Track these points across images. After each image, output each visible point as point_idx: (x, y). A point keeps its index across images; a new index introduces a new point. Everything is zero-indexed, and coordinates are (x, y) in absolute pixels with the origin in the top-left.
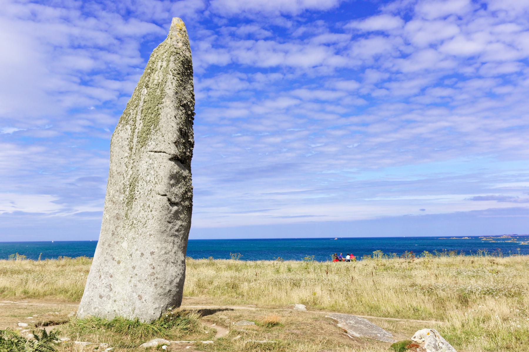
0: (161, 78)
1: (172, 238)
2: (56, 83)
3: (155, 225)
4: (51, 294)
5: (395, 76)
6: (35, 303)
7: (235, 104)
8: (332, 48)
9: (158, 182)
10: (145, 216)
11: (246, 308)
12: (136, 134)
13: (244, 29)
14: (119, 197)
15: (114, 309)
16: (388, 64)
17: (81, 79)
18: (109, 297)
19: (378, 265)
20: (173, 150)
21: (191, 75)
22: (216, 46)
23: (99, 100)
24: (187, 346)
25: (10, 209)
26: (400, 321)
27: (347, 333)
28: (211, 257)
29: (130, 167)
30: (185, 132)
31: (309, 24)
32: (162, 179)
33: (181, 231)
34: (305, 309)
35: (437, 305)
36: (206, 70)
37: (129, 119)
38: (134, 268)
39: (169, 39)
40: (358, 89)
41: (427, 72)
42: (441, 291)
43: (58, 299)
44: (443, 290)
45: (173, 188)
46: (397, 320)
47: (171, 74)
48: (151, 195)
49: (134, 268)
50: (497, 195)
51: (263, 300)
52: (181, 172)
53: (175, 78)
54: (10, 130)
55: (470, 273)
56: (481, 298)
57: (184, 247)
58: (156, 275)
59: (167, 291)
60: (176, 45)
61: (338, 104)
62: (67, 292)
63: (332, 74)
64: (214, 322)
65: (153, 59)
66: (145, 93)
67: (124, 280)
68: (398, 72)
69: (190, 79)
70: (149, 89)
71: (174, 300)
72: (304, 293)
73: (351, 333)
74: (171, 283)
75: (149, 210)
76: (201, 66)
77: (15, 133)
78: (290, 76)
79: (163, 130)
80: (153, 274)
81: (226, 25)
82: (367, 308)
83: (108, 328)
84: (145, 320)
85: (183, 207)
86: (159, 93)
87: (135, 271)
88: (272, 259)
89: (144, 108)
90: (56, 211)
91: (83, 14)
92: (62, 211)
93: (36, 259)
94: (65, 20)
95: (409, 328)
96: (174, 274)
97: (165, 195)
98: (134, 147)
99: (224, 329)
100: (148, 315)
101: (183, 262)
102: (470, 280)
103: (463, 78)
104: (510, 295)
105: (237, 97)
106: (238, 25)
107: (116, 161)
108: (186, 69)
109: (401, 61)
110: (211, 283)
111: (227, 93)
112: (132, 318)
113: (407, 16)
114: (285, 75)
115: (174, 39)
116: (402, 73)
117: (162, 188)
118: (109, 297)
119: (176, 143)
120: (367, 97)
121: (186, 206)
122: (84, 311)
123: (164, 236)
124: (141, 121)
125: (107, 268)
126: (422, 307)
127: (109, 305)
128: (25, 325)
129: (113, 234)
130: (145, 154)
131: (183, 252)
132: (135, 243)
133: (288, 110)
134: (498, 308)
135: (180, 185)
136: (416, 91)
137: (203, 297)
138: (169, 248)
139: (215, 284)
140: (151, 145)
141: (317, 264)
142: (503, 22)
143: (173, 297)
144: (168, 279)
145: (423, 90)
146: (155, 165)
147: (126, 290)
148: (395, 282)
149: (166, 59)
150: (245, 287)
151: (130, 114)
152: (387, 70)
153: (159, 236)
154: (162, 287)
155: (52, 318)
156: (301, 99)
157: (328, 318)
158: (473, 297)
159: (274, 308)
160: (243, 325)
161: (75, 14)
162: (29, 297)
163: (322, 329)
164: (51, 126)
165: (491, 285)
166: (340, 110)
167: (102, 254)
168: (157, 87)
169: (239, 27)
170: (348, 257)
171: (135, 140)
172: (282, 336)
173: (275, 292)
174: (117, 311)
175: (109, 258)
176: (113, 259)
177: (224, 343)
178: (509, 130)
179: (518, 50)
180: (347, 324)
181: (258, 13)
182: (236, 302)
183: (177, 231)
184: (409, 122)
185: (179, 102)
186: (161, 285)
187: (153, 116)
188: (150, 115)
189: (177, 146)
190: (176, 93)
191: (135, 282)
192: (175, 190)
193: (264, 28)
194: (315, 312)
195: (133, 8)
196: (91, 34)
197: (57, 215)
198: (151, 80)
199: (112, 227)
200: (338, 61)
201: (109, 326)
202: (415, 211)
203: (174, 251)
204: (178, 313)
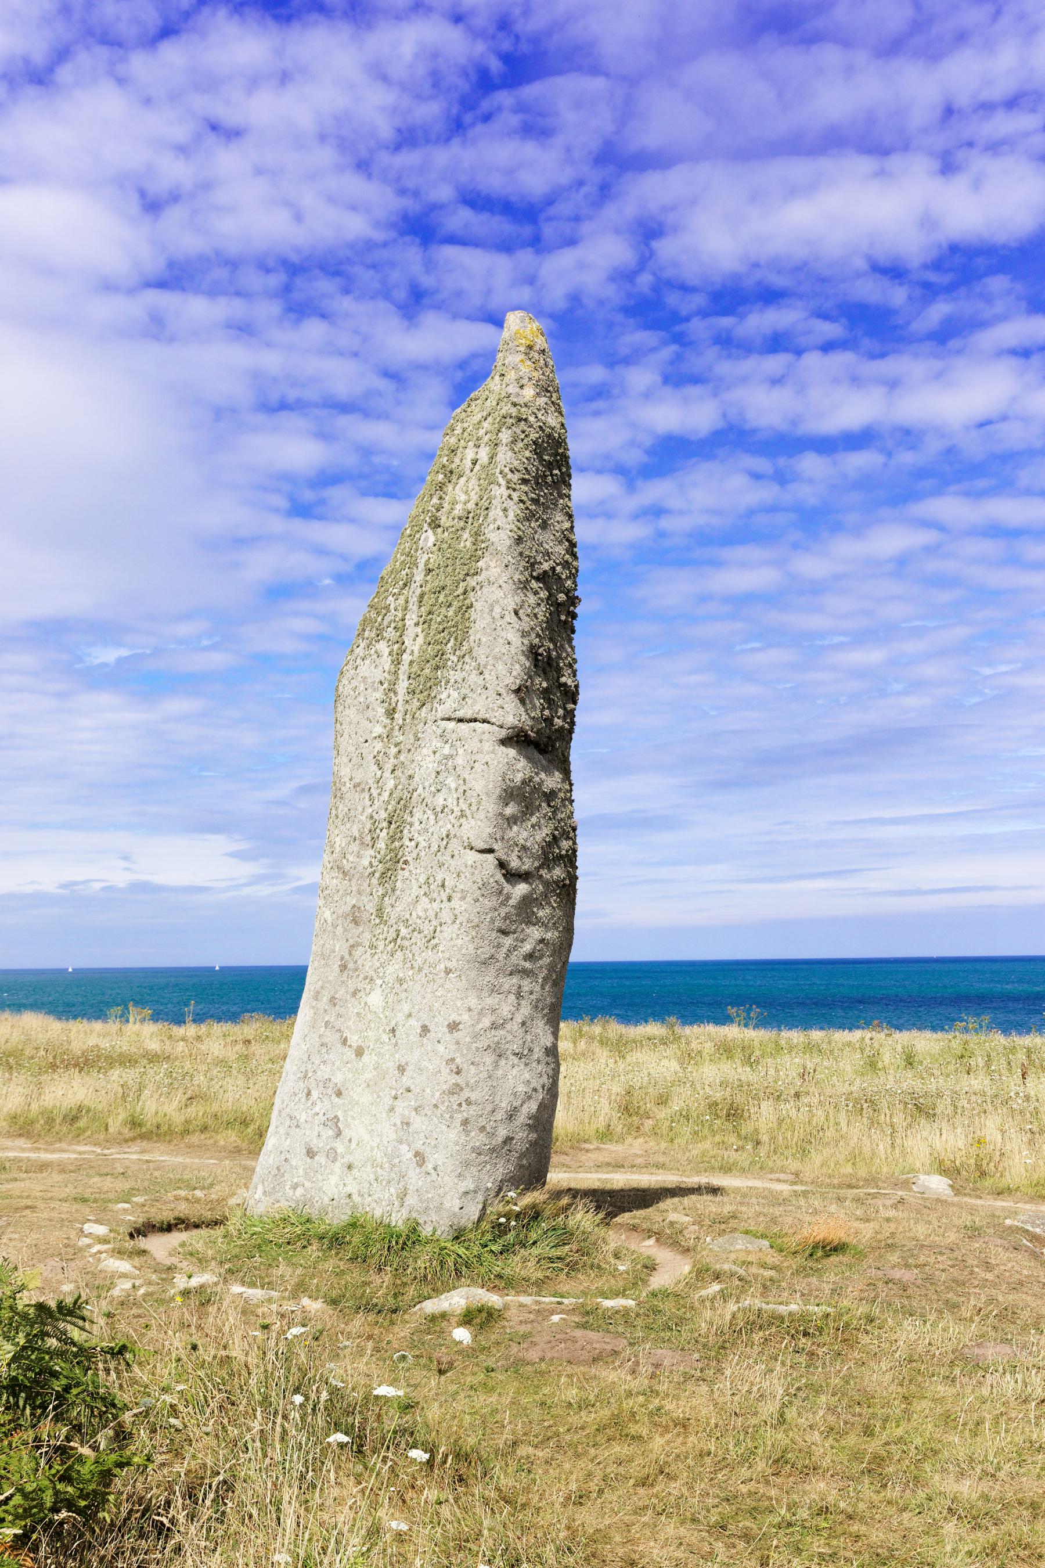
0: (475, 498)
1: (515, 980)
2: (226, 514)
3: (460, 942)
4: (205, 1129)
6: (161, 1155)
7: (739, 552)
9: (468, 813)
10: (431, 914)
11: (758, 1184)
12: (404, 668)
15: (349, 1189)
17: (292, 499)
18: (333, 1155)
20: (512, 714)
22: (678, 379)
23: (344, 558)
24: (552, 1312)
28: (673, 1019)
29: (388, 767)
30: (549, 657)
31: (962, 291)
32: (479, 803)
33: (541, 958)
34: (949, 1192)
36: (648, 452)
37: (385, 623)
38: (402, 1069)
39: (497, 377)
43: (222, 1143)
45: (515, 828)
48: (449, 850)
49: (402, 1069)
52: (537, 779)
54: (110, 655)
58: (466, 1094)
59: (500, 1140)
62: (245, 1123)
64: (649, 1233)
65: (453, 440)
67: (375, 1105)
69: (561, 496)
70: (440, 530)
71: (521, 1166)
72: (952, 1140)
74: (511, 1116)
75: (444, 896)
76: (633, 443)
77: (120, 661)
78: (907, 458)
79: (481, 653)
80: (456, 1089)
81: (703, 313)
83: (330, 1249)
84: (435, 1225)
85: (547, 884)
86: (468, 544)
87: (405, 1079)
88: (868, 1025)
89: (426, 589)
90: (243, 881)
91: (290, 309)
94: (240, 329)
96: (521, 1089)
97: (491, 851)
98: (400, 707)
99: (679, 1257)
100: (446, 1214)
101: (552, 1052)
105: (742, 532)
106: (741, 309)
107: (351, 749)
108: (550, 466)
110: (663, 1101)
112: (398, 1220)
114: (890, 455)
115: (511, 376)
117: (478, 828)
118: (333, 1155)
119: (521, 692)
121: (556, 882)
124: (419, 629)
125: (328, 1070)
127: (334, 1180)
128: (101, 1230)
129: (343, 968)
130: (430, 728)
131: (547, 1022)
132: (403, 995)
133: (902, 563)
135: (534, 820)
137: (636, 1146)
138: (505, 1010)
140: (448, 701)
141: (999, 1039)
143: (520, 1158)
144: (503, 1105)
146: (460, 761)
147: (381, 1136)
149: (486, 438)
150: (764, 1116)
151: (387, 608)
153: (473, 974)
154: (483, 1129)
155: (183, 1209)
159: (850, 1186)
160: (731, 1251)
161: (269, 310)
162: (142, 1137)
163: (988, 1266)
164: (217, 639)
168: (462, 523)
169: (742, 317)
171: (403, 686)
172: (853, 1291)
173: (856, 1131)
174: (355, 1197)
175: (332, 1037)
176: (345, 1042)
177: (668, 1307)
181: (799, 268)
182: (735, 1163)
183: (530, 957)
185: (526, 568)
186: (482, 1122)
187: (451, 613)
188: (443, 610)
189: (522, 701)
190: (519, 540)
191: (406, 1112)
192: (520, 833)
193: (824, 316)
194: (979, 1202)
195: (427, 281)
196: (313, 365)
197: (246, 891)
198: (446, 505)
199: (341, 947)
201: (335, 1241)
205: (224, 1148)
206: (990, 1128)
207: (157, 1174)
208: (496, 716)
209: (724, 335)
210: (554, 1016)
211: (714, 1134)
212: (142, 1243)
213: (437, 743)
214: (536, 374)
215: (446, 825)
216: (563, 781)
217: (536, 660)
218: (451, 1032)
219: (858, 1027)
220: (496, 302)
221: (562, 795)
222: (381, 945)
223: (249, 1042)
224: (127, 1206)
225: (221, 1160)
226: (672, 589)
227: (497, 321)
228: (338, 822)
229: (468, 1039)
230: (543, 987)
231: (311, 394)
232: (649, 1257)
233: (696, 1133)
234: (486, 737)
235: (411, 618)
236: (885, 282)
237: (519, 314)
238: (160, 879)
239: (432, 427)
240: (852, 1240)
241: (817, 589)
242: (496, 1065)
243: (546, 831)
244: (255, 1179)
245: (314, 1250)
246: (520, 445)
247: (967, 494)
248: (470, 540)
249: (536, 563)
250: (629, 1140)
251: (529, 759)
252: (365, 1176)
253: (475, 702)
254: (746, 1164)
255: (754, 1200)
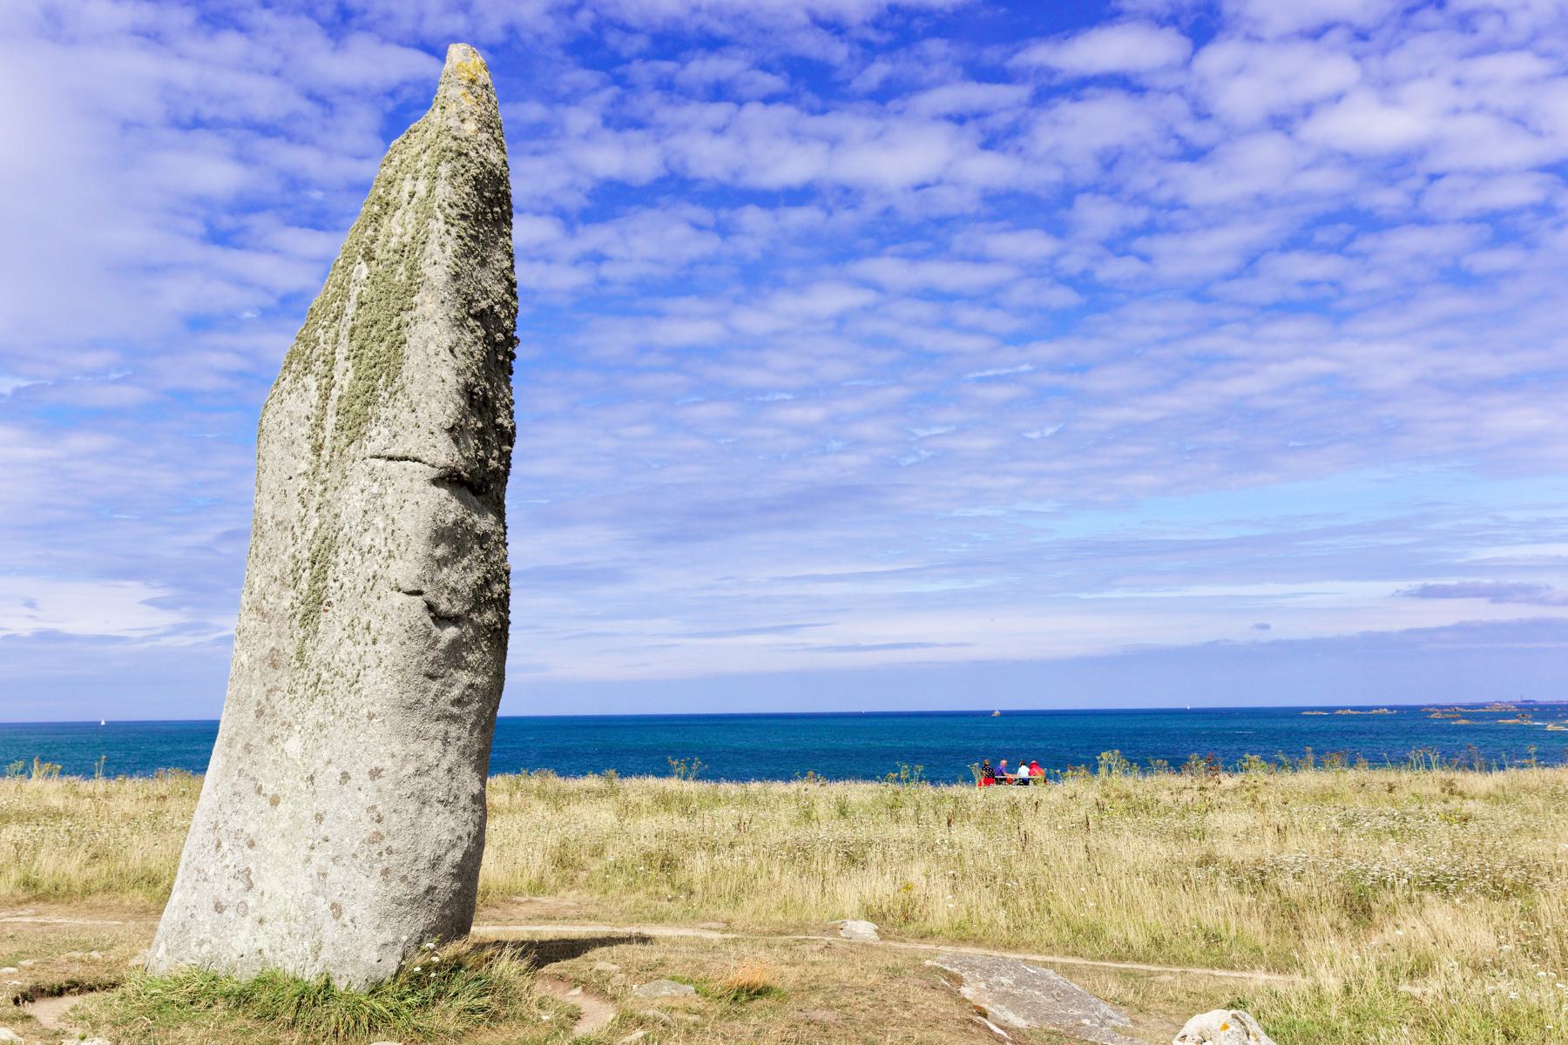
0: (411, 231)
1: (442, 726)
2: (132, 237)
3: (384, 686)
4: (108, 888)
5: (1167, 218)
6: (59, 918)
8: (971, 128)
9: (396, 553)
10: (355, 657)
11: (689, 932)
12: (333, 403)
13: (702, 68)
14: (279, 597)
15: (259, 945)
16: (1143, 180)
19: (1107, 796)
20: (444, 453)
21: (505, 220)
22: (619, 122)
23: (268, 291)
25: (22, 624)
26: (1160, 973)
27: (985, 1016)
29: (313, 505)
30: (485, 396)
31: (901, 52)
33: (469, 703)
34: (875, 936)
35: (1276, 923)
36: (589, 197)
37: (314, 356)
38: (319, 818)
39: (438, 110)
40: (1053, 259)
41: (1262, 202)
42: (1290, 879)
43: (128, 903)
44: (1298, 877)
45: (445, 570)
46: (1153, 968)
47: (441, 217)
49: (319, 818)
50: (1487, 581)
51: (748, 906)
52: (469, 521)
53: (453, 231)
55: (1382, 822)
56: (1410, 901)
57: (482, 754)
58: (387, 842)
59: (422, 889)
60: (459, 129)
61: (994, 305)
63: (971, 210)
64: (576, 983)
65: (390, 172)
66: (363, 276)
67: (292, 857)
68: (1174, 205)
69: (502, 234)
71: (444, 917)
72: (878, 886)
73: (1001, 1016)
74: (434, 864)
75: (369, 639)
76: (571, 186)
77: (17, 392)
80: (377, 838)
81: (646, 57)
82: (1065, 931)
83: (237, 1007)
84: (350, 980)
85: (477, 628)
87: (322, 828)
92: (179, 629)
93: (89, 774)
94: (148, 36)
95: (1182, 996)
96: (446, 837)
97: (419, 593)
98: (327, 443)
101: (479, 799)
102: (1382, 843)
103: (1371, 223)
104: (1499, 891)
105: (683, 282)
107: (274, 486)
108: (490, 203)
109: (1182, 169)
110: (598, 852)
111: (657, 271)
112: (311, 976)
113: (1203, 27)
114: (830, 213)
116: (1185, 207)
117: (407, 569)
120: (1082, 283)
122: (168, 951)
123: (415, 721)
124: (349, 364)
126: (1233, 926)
127: (243, 935)
129: (260, 713)
130: (359, 465)
132: (323, 741)
133: (841, 321)
134: (1460, 929)
135: (465, 562)
136: (1227, 263)
137: (569, 898)
138: (431, 756)
139: (611, 856)
141: (928, 791)
142: (1492, 48)
145: (1251, 263)
146: (389, 500)
148: (1157, 851)
149: (425, 171)
150: (698, 866)
151: (316, 341)
152: (1140, 199)
153: (398, 718)
154: (404, 879)
155: (77, 972)
156: (878, 288)
157: (933, 970)
158: (1387, 897)
159: (780, 933)
162: (38, 899)
163: (906, 1005)
165: (1441, 861)
166: (1000, 322)
167: (226, 774)
168: (397, 257)
169: (684, 64)
170: (1024, 771)
171: (331, 421)
173: (787, 879)
174: (266, 953)
175: (245, 786)
176: (259, 790)
178: (1512, 384)
179: (1539, 134)
180: (990, 987)
183: (458, 702)
184: (1208, 360)
185: (463, 306)
187: (383, 349)
188: (375, 345)
189: (456, 441)
190: (456, 277)
191: (323, 863)
192: (451, 576)
193: (766, 68)
194: (903, 946)
196: (228, 82)
199: (258, 692)
200: (991, 169)
201: (243, 999)
202: (1238, 630)
203: (445, 765)
204: (457, 957)
205: (129, 908)
206: (916, 873)
207: (51, 936)
208: (428, 455)
209: (665, 80)
210: (486, 764)
211: (647, 884)
212: (28, 1008)
213: (365, 481)
214: (478, 109)
215: (371, 566)
216: (497, 523)
217: (471, 399)
218: (373, 779)
219: (796, 779)
220: (431, 27)
221: (495, 537)
222: (300, 689)
223: (164, 798)
224: (12, 970)
225: (125, 921)
226: (613, 338)
227: (439, 53)
228: (258, 561)
229: (390, 786)
230: (471, 734)
231: (229, 113)
232: (573, 1006)
233: (629, 885)
234: (418, 475)
235: (342, 352)
236: (826, 37)
237: (463, 47)
238: (68, 628)
239: (362, 157)
240: (778, 984)
241: (759, 344)
242: (420, 812)
243: (478, 574)
244: (158, 937)
245: (220, 1009)
246: (460, 179)
247: (903, 256)
248: (406, 274)
249: (473, 300)
250: (562, 892)
251: (461, 500)
252: (277, 931)
253: (406, 440)
254: (678, 914)
255: (683, 948)
